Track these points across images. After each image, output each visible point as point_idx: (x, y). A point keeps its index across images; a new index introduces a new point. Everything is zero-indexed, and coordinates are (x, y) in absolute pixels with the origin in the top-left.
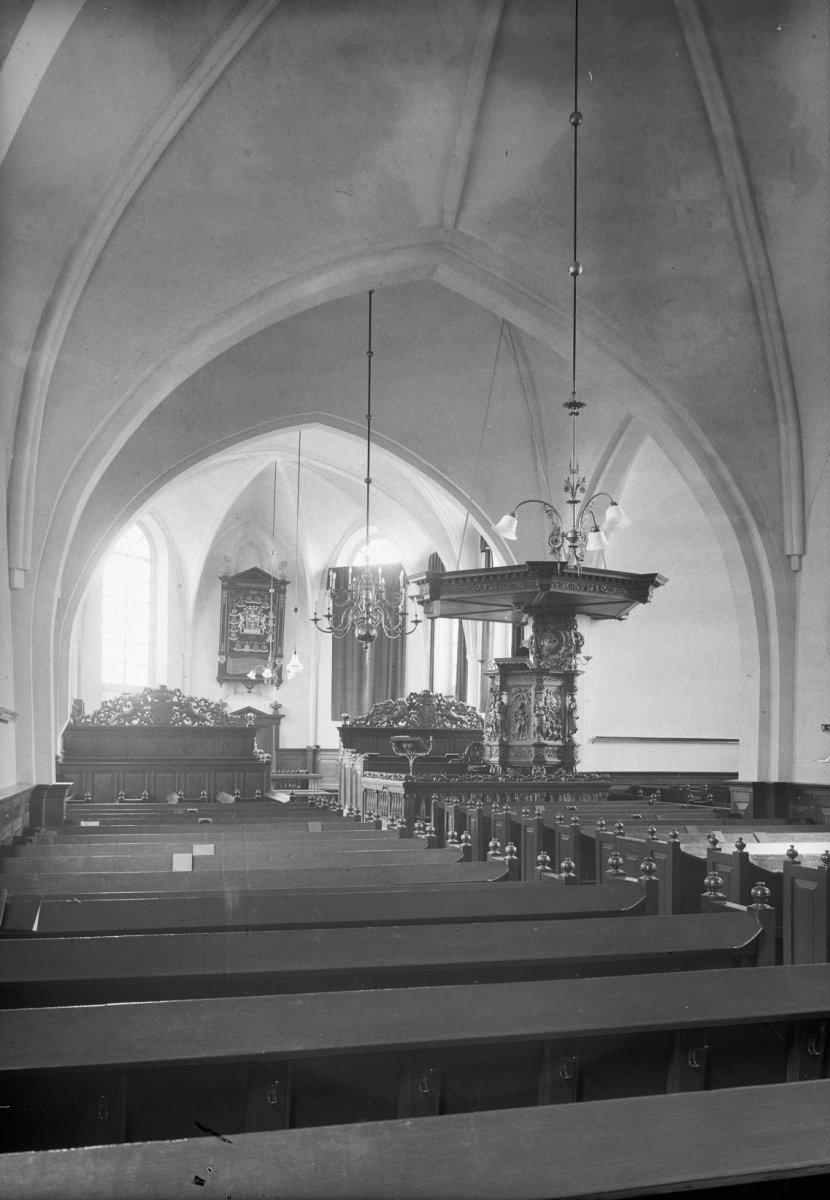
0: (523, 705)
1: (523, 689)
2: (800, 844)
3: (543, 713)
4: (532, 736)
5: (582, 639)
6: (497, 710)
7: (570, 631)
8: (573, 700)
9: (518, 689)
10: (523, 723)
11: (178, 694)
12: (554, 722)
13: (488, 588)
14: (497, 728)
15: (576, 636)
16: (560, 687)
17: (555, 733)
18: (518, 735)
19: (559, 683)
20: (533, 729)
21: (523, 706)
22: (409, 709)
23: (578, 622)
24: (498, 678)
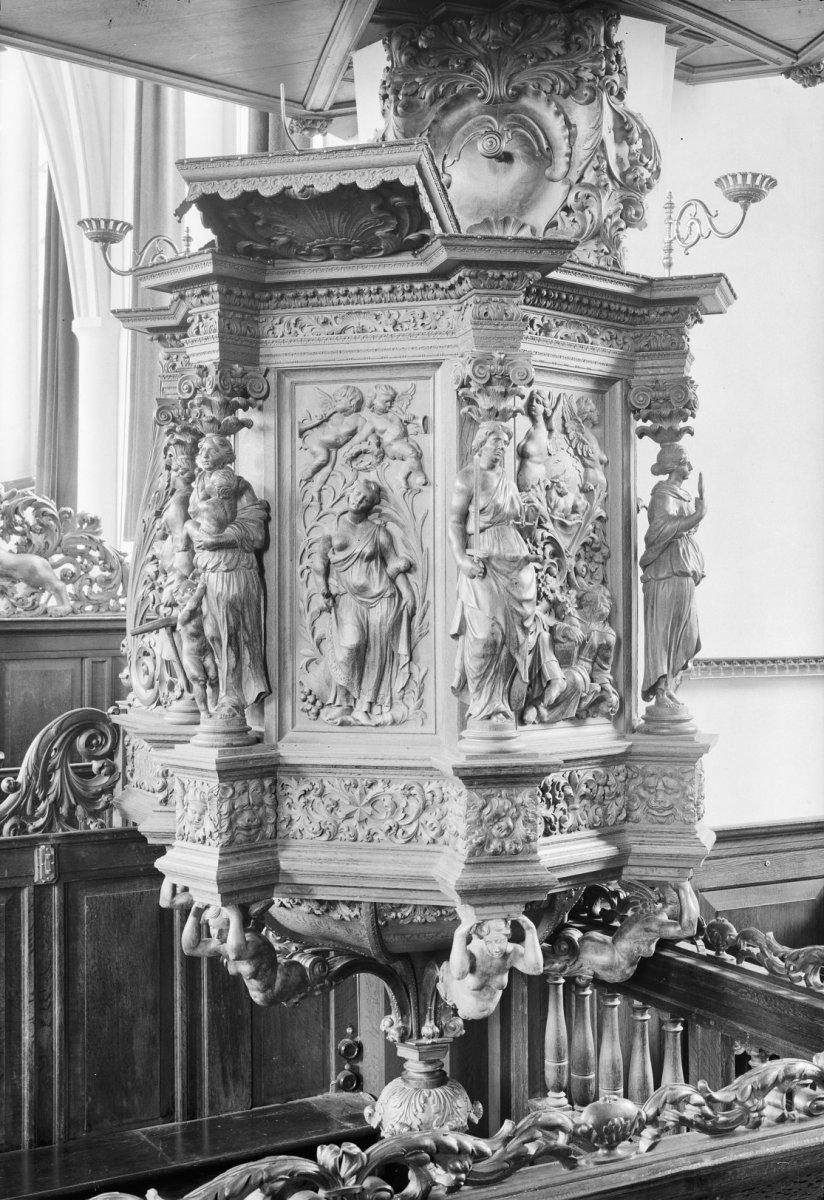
1: (374, 391)
2: (707, 805)
3: (522, 549)
5: (649, 148)
6: (203, 530)
8: (672, 467)
9: (337, 391)
12: (569, 599)
14: (204, 650)
16: (602, 384)
17: (581, 672)
19: (598, 358)
21: (369, 508)
23: (629, 54)
24: (208, 312)
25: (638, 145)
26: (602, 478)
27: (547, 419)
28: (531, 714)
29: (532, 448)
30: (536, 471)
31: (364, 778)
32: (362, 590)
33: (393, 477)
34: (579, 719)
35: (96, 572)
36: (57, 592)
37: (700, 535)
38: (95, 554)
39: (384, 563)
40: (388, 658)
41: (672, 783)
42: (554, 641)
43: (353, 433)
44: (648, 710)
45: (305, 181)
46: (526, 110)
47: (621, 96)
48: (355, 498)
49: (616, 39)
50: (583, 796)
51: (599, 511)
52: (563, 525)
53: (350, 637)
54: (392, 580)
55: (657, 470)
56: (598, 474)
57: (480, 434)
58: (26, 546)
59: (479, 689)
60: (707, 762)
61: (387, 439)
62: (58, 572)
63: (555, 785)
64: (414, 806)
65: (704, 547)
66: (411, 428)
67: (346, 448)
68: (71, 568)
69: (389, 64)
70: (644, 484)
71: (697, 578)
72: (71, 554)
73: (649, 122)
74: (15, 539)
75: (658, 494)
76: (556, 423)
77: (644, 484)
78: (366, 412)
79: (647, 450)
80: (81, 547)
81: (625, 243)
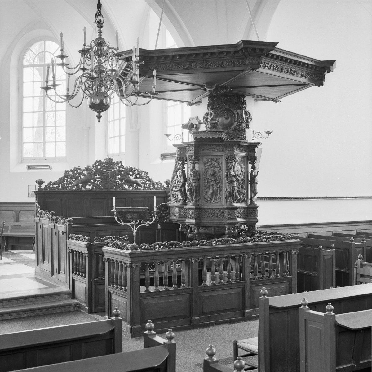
0: (215, 172)
4: (223, 200)
5: (250, 116)
7: (241, 109)
8: (253, 168)
10: (215, 188)
11: (120, 165)
13: (196, 65)
15: (246, 113)
18: (211, 199)
19: (243, 154)
20: (224, 194)
22: (95, 174)
23: (247, 102)
25: (248, 116)
26: (244, 170)
27: (237, 162)
28: (235, 202)
29: (235, 166)
30: (236, 169)
31: (213, 210)
32: (213, 185)
33: (217, 170)
34: (241, 203)
35: (147, 182)
36: (141, 186)
37: (257, 177)
38: (147, 179)
39: (216, 182)
40: (216, 194)
41: (253, 212)
42: (238, 192)
43: (211, 164)
44: (250, 202)
45: (208, 136)
46: (231, 111)
47: (246, 109)
48: (212, 173)
49: (245, 99)
50: (242, 213)
51: (244, 174)
52: (239, 176)
53: (211, 191)
54: (217, 184)
55: (251, 168)
56: (243, 169)
57: (229, 165)
58: (136, 178)
59: (229, 198)
60: (258, 209)
61: (216, 165)
62: (141, 182)
63: (238, 211)
64: (220, 213)
65: (258, 179)
66: (219, 164)
67: (211, 166)
68: (143, 181)
69: (209, 102)
70: (250, 170)
71: (257, 183)
72: (143, 179)
73: (250, 112)
74: (134, 176)
75: (252, 172)
76: (238, 163)
77: (250, 170)
78: (213, 161)
79: (250, 166)
80: (145, 178)
81: (246, 131)
